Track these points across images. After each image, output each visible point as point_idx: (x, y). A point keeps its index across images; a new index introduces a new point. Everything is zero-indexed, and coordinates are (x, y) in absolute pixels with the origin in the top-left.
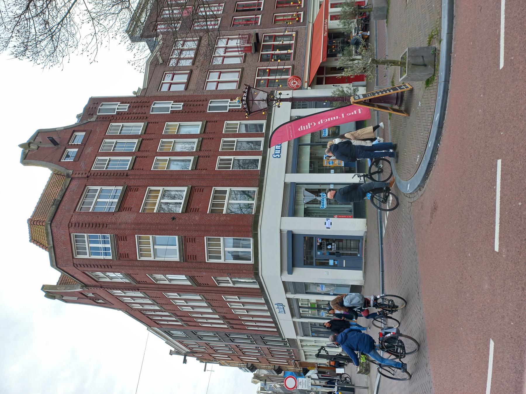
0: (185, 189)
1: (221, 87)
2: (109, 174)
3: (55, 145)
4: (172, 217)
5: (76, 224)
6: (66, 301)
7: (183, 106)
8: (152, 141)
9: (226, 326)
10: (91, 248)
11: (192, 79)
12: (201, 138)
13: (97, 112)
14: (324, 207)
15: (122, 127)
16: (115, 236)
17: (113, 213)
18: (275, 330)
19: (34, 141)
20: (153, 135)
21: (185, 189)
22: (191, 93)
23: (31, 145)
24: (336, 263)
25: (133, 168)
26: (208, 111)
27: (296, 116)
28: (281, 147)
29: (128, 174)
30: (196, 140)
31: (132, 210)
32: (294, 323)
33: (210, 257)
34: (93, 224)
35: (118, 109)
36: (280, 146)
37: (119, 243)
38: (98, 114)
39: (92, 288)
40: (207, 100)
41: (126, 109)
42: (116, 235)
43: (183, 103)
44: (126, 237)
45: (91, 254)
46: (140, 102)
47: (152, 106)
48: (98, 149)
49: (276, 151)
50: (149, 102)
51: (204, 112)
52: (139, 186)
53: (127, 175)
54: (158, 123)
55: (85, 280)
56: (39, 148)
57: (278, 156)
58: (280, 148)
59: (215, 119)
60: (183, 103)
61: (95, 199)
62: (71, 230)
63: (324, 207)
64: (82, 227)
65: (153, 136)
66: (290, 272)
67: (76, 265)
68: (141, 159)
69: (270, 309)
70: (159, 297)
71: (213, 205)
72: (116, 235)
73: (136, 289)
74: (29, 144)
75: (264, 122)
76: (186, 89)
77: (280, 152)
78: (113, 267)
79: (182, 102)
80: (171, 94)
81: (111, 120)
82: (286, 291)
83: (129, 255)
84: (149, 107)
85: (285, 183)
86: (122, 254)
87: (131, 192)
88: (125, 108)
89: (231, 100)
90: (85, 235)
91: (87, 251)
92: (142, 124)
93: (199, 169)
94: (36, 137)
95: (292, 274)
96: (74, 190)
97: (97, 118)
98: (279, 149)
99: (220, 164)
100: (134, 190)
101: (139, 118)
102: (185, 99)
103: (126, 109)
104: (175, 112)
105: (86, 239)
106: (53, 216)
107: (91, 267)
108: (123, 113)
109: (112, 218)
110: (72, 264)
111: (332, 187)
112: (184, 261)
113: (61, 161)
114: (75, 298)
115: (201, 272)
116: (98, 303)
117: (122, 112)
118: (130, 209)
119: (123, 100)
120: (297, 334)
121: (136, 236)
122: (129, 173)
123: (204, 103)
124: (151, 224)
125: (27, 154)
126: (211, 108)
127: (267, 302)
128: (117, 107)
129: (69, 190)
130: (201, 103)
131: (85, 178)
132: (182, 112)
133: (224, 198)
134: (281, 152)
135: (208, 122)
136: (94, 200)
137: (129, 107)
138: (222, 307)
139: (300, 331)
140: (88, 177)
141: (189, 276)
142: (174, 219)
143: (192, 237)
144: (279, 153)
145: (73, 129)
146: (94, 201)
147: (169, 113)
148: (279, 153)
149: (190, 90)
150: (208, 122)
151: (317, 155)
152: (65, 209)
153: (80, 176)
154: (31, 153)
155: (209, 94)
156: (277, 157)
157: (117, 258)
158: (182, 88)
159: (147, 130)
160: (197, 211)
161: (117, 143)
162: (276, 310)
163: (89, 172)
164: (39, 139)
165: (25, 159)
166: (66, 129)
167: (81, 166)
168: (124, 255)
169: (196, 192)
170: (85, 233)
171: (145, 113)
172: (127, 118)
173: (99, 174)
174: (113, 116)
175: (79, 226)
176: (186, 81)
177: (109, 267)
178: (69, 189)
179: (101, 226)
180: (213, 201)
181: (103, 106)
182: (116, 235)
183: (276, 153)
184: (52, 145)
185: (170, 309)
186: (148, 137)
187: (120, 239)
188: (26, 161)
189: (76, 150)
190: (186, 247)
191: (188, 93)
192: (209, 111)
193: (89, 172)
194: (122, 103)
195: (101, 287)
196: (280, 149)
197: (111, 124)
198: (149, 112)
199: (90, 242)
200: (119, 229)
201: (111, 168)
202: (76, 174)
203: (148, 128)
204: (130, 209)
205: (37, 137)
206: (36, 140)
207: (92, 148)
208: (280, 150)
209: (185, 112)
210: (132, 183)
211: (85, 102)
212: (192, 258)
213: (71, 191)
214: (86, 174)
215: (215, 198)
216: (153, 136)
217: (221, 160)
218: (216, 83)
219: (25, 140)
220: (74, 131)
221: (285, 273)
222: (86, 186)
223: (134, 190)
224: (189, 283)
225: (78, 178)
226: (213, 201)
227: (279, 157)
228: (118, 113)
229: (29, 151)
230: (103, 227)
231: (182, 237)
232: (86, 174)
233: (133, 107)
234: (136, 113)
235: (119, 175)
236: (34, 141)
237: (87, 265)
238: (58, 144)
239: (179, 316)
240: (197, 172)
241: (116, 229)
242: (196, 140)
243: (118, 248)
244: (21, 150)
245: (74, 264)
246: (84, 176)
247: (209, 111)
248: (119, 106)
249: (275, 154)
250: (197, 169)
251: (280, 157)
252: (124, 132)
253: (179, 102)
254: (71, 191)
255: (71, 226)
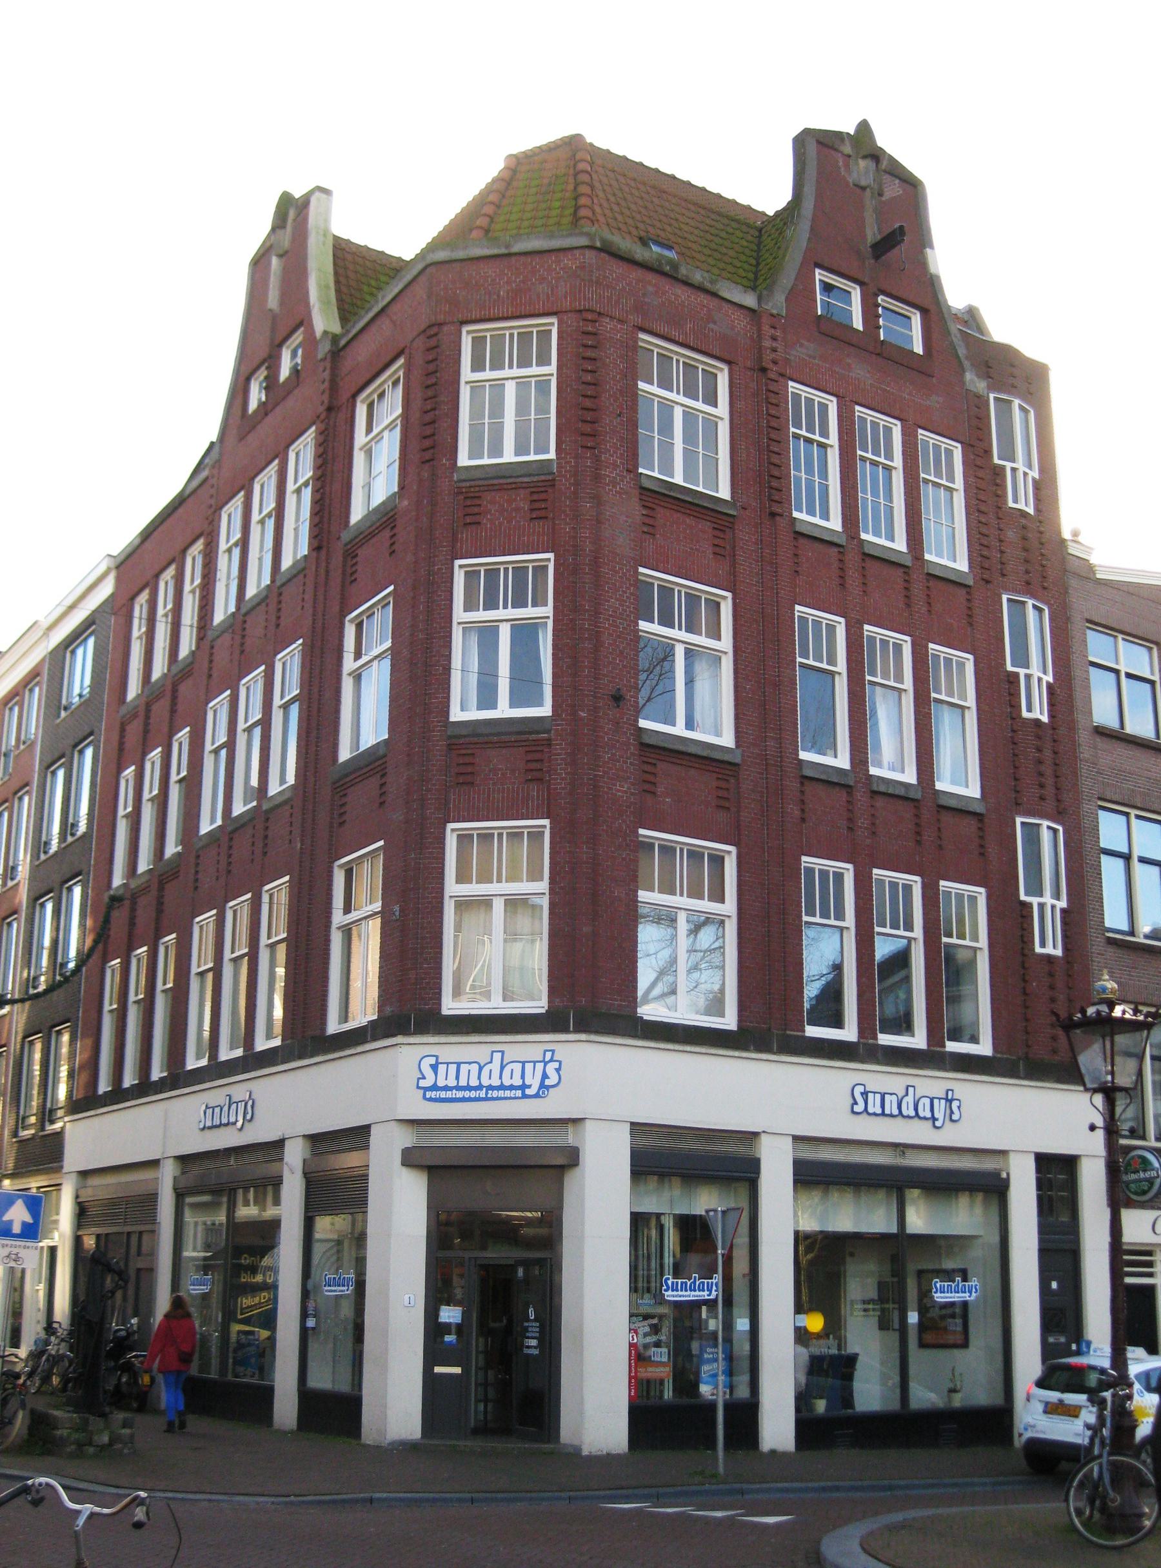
0: (727, 740)
1: (1111, 870)
2: (776, 449)
3: (871, 247)
4: (624, 691)
5: (591, 337)
6: (259, 263)
7: (1037, 722)
8: (901, 605)
9: (118, 881)
10: (498, 387)
11: (1138, 753)
12: (919, 796)
13: (999, 391)
14: (670, 1293)
15: (948, 489)
16: (550, 478)
17: (632, 469)
18: (104, 1087)
19: (885, 171)
20: (924, 609)
21: (727, 740)
22: (1085, 753)
23: (871, 165)
24: (448, 1338)
25: (804, 537)
26: (1019, 820)
27: (1008, 1174)
28: (891, 1116)
29: (778, 518)
30: (910, 776)
31: (648, 536)
32: (154, 1164)
33: (464, 839)
34: (595, 397)
35: (1014, 470)
36: (895, 1112)
37: (522, 493)
38: (992, 396)
39: (327, 375)
40: (1058, 815)
41: (1016, 501)
42: (552, 483)
43: (1045, 719)
44: (546, 518)
45: (476, 387)
46: (1042, 555)
47: (1030, 602)
48: (863, 402)
49: (878, 1097)
50: (1045, 588)
51: (1017, 804)
52: (733, 565)
53: (773, 515)
54: (971, 625)
55: (363, 352)
56: (858, 191)
57: (858, 1107)
58: (887, 1111)
59: (993, 850)
60: (1045, 719)
61: (681, 399)
62: (571, 319)
63: (666, 1290)
64: (584, 358)
65: (920, 606)
66: (410, 1159)
67: (436, 335)
68: (836, 564)
69: (218, 1070)
70: (278, 626)
71: (667, 850)
72: (554, 480)
73: (321, 541)
74: (876, 155)
75: (984, 1048)
76: (1102, 732)
77: (875, 1114)
78: (426, 466)
79: (1052, 716)
80: (1077, 673)
81: (973, 446)
82: (319, 1141)
83: (474, 527)
84: (1028, 588)
85: (756, 1134)
86: (478, 502)
87: (710, 530)
88: (1021, 500)
89: (1063, 911)
90: (552, 368)
91: (488, 374)
92: (962, 565)
93: (802, 792)
94: (900, 179)
95: (403, 1164)
96: (715, 323)
97: (978, 397)
98: (916, 1109)
99: (824, 874)
100: (716, 541)
101: (985, 553)
102: (1062, 731)
103: (1016, 501)
104: (1012, 691)
105: (535, 370)
106: (620, 253)
107: (427, 387)
108: (999, 492)
109: (615, 466)
110: (441, 318)
111: (742, 1324)
112: (450, 737)
113: (817, 271)
114: (273, 300)
115: (407, 803)
116: (248, 380)
117: (1002, 486)
118: (651, 530)
119: (1045, 489)
120: (84, 1174)
121: (551, 556)
122: (782, 522)
123: (1050, 805)
124: (597, 613)
125: (836, 150)
126: (1032, 832)
127: (254, 1061)
128: (1020, 465)
129: (713, 303)
130: (1050, 791)
131: (760, 358)
132: (1013, 719)
133: (695, 893)
134: (874, 1118)
135: (981, 821)
136: (678, 393)
137: (1024, 514)
138: (229, 872)
139: (101, 1188)
140: (764, 370)
141: (385, 756)
142: (617, 698)
143: (548, 772)
144: (871, 1110)
145: (933, 308)
146: (672, 396)
147: (1009, 668)
148: (871, 1110)
149: (1095, 748)
150: (981, 821)
151: (848, 1259)
152: (644, 295)
153: (767, 343)
154: (841, 164)
155: (1086, 822)
156: (856, 1103)
157: (464, 484)
158: (1103, 711)
159: (941, 584)
160: (647, 786)
161: (887, 472)
162: (214, 1095)
163: (782, 375)
164: (893, 190)
165: (819, 142)
166: (932, 285)
167: (802, 345)
168: (476, 510)
169: (715, 784)
170: (559, 368)
171: (1003, 575)
172: (983, 508)
173: (773, 412)
174: (988, 452)
175: (585, 346)
176: (1129, 729)
177: (428, 455)
178: (716, 301)
179: (588, 428)
180: (682, 850)
181: (1023, 415)
182: (552, 483)
183: (870, 1096)
184: (872, 234)
185: (216, 658)
186: (917, 589)
187: (535, 497)
188: (812, 148)
189: (858, 324)
190: (505, 745)
191: (1084, 737)
192: (1023, 823)
193: (782, 375)
194: (1037, 485)
195: (330, 409)
196: (883, 1114)
197: (959, 445)
198: (1007, 590)
199: (522, 384)
200: (575, 493)
201: (797, 453)
202: (775, 328)
203: (951, 588)
204: (651, 530)
205: (897, 181)
206: (887, 178)
207: (870, 382)
208: (879, 1111)
209: (1015, 728)
210: (745, 535)
211: (1030, 348)
212: (463, 769)
213: (709, 310)
214: (775, 362)
215: (695, 855)
216: (920, 606)
217: (839, 877)
218: (1125, 850)
219: (884, 140)
220: (924, 312)
221: (405, 1139)
222: (729, 362)
223: (716, 541)
224: (91, 642)
225: (760, 336)
226: (682, 850)
227: (857, 1109)
228: (999, 472)
229: (849, 156)
230: (583, 434)
231: (548, 732)
232: (775, 362)
233: (1024, 527)
234: (1001, 541)
235: (774, 484)
236: (885, 171)
237: (436, 372)
238: (877, 257)
239: (175, 691)
240: (793, 785)
241: (576, 484)
242: (910, 776)
243: (501, 488)
244: (849, 127)
245: (441, 324)
246: (768, 356)
247: (1023, 823)
248: (1025, 474)
249: (865, 1094)
250: (802, 784)
251: (853, 1112)
252: (928, 494)
253: (1051, 705)
254: (709, 310)
255: (585, 320)
